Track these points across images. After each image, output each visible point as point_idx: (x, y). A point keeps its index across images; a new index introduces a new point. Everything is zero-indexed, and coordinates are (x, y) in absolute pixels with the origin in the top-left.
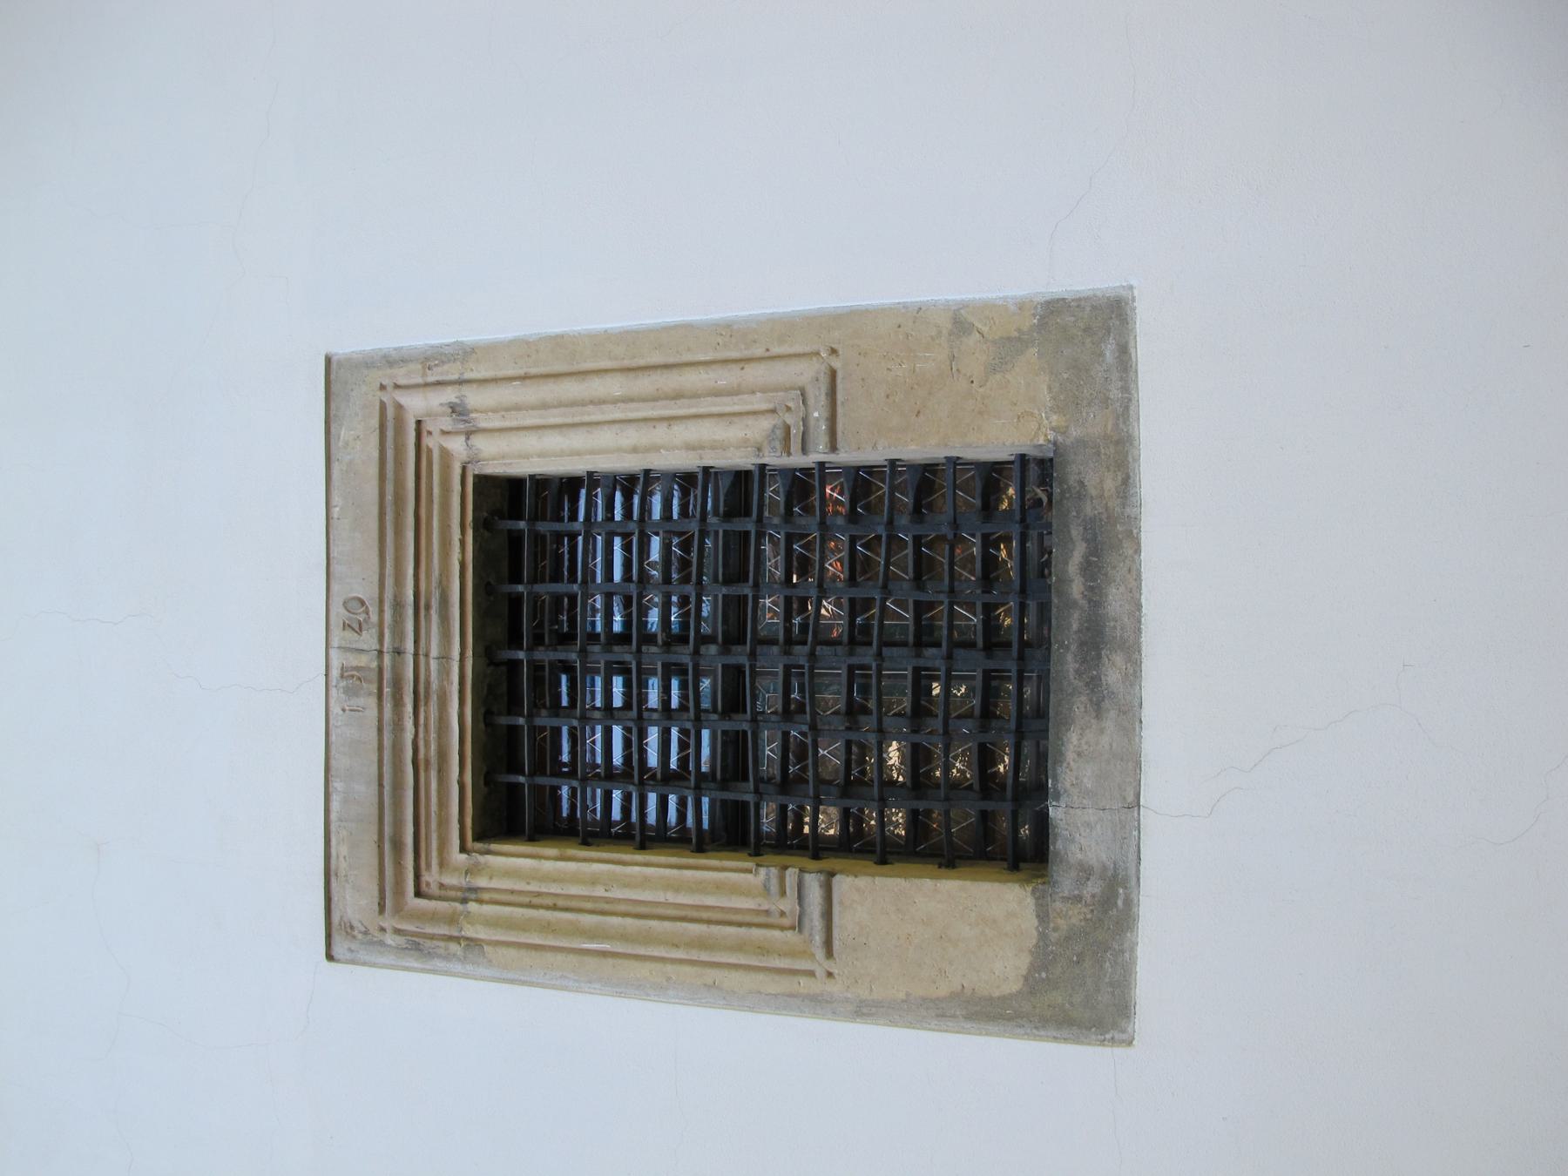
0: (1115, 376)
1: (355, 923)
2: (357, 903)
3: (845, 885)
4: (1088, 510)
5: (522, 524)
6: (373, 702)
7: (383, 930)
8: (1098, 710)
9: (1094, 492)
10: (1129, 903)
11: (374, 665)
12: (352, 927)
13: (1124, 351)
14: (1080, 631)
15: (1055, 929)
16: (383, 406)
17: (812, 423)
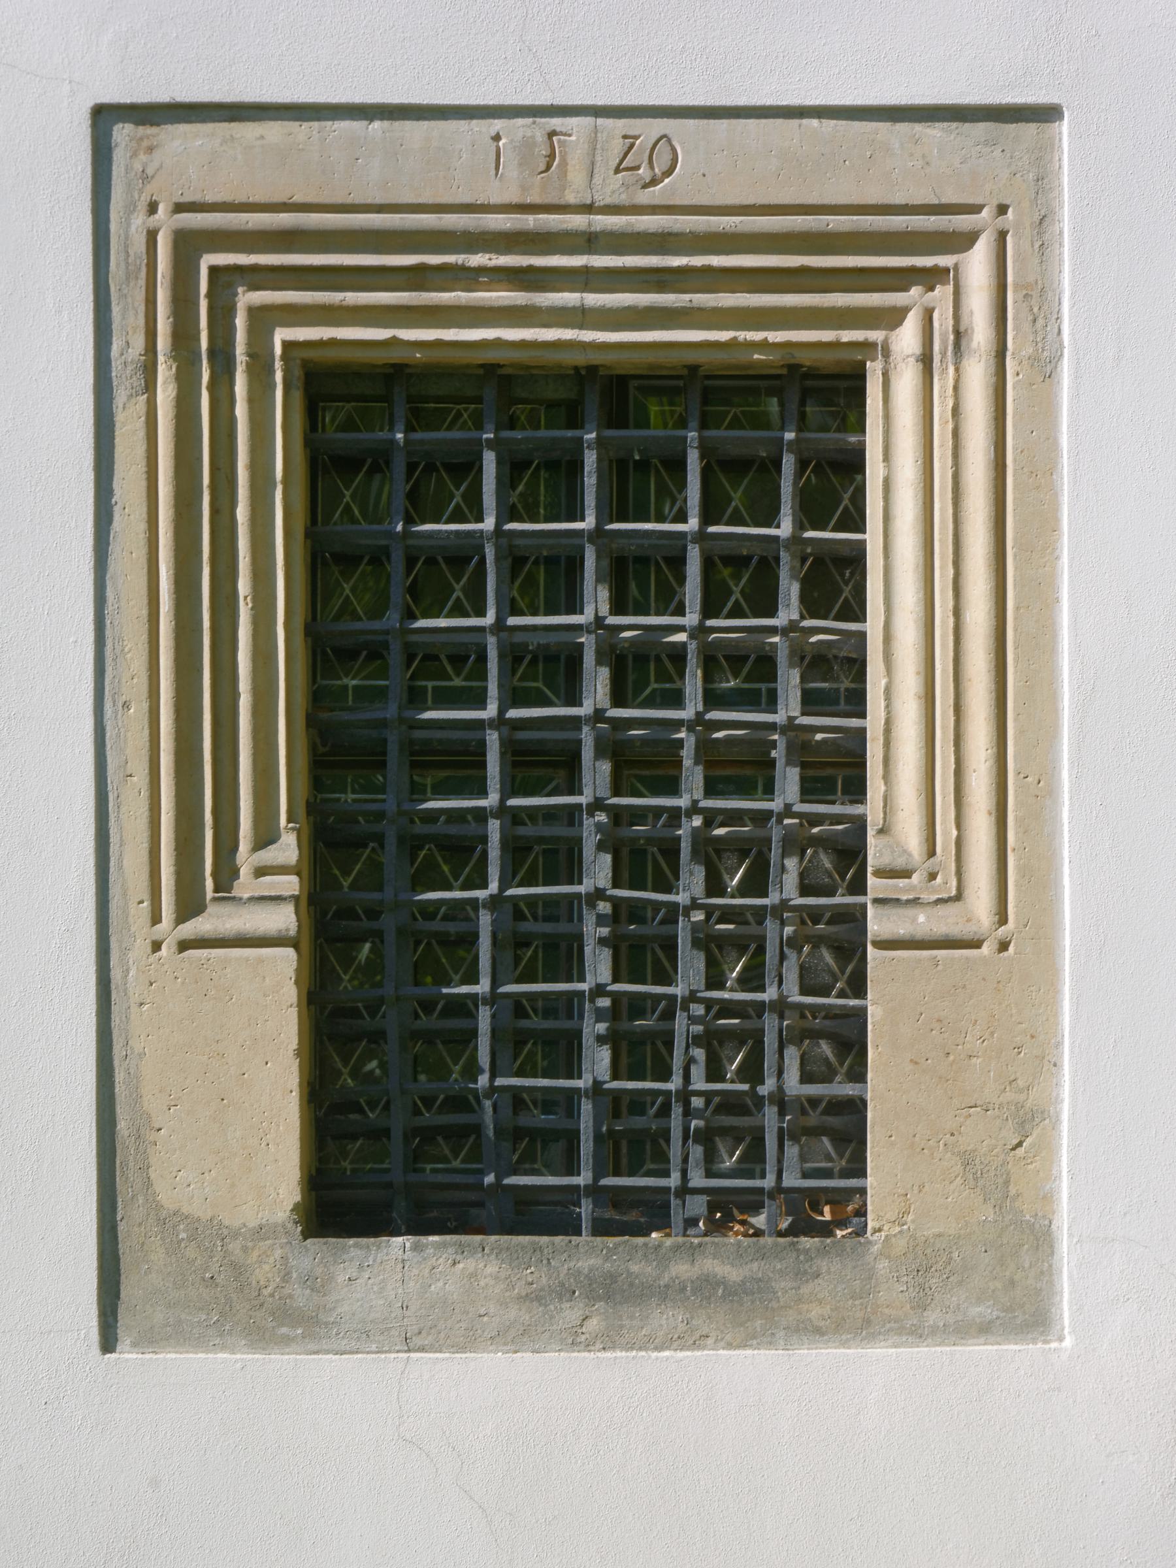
0: (950, 1318)
1: (157, 155)
2: (189, 161)
3: (284, 964)
4: (781, 1285)
5: (785, 431)
6: (511, 196)
7: (152, 208)
8: (535, 1298)
9: (806, 1290)
10: (285, 1342)
11: (571, 198)
12: (150, 149)
13: (985, 1330)
14: (630, 1274)
15: (245, 1249)
16: (976, 209)
17: (910, 912)
